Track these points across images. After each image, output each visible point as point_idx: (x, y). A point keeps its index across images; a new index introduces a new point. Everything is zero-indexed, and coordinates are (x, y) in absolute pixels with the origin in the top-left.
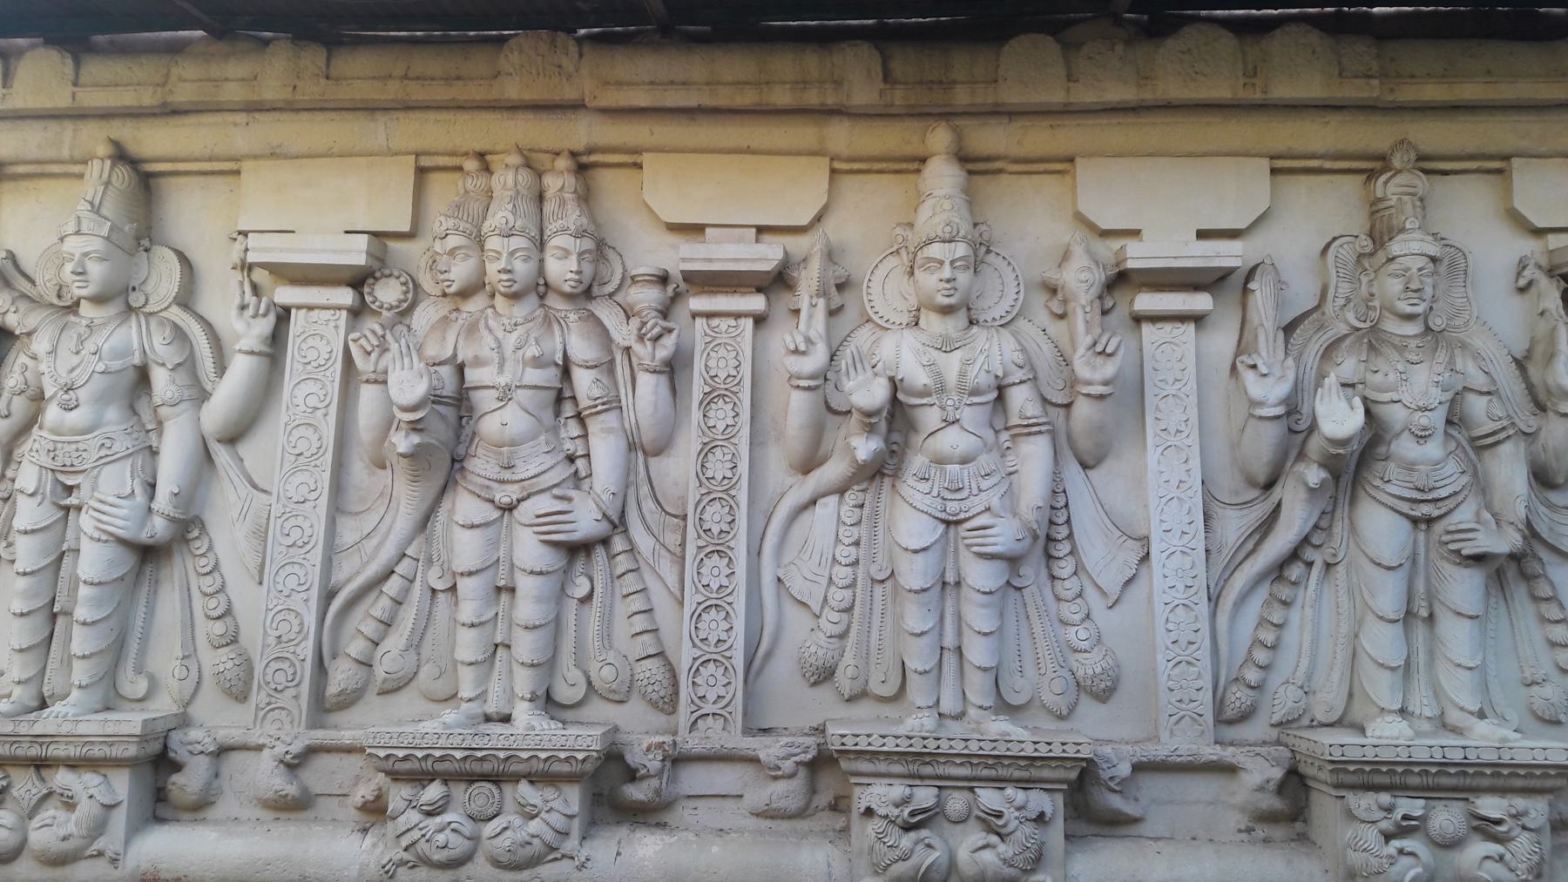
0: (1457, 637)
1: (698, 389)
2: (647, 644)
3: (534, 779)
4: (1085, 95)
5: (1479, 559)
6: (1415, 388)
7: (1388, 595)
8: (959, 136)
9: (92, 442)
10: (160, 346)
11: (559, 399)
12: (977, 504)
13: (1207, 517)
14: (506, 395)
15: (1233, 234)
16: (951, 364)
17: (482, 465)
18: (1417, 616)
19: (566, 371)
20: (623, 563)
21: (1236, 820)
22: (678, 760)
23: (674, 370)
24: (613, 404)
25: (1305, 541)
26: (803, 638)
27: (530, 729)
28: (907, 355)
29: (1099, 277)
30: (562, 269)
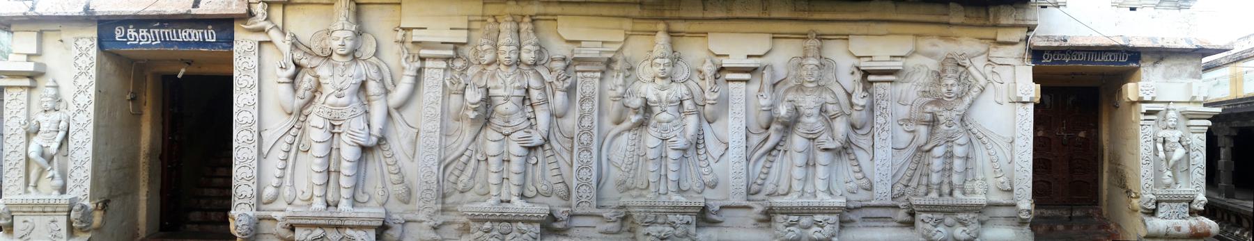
0: (821, 171)
1: (578, 97)
2: (559, 179)
3: (523, 222)
4: (709, 15)
5: (826, 150)
6: (808, 102)
7: (800, 159)
8: (668, 25)
9: (349, 109)
10: (373, 73)
11: (524, 99)
12: (672, 134)
13: (747, 138)
14: (507, 99)
15: (759, 56)
16: (664, 94)
17: (497, 121)
18: (810, 164)
19: (527, 91)
20: (548, 153)
21: (752, 221)
22: (572, 216)
23: (570, 91)
24: (546, 101)
25: (778, 144)
26: (614, 174)
27: (518, 205)
28: (650, 91)
29: (714, 69)
30: (528, 56)
